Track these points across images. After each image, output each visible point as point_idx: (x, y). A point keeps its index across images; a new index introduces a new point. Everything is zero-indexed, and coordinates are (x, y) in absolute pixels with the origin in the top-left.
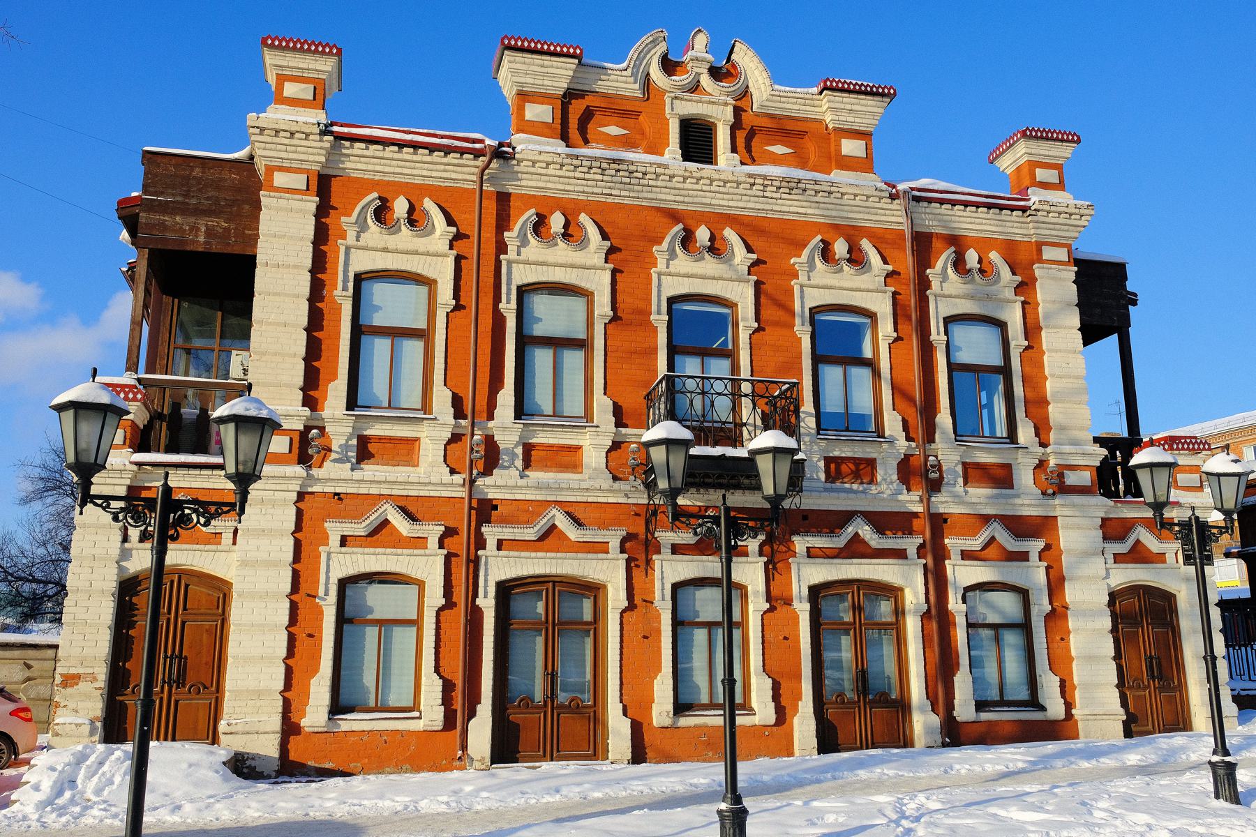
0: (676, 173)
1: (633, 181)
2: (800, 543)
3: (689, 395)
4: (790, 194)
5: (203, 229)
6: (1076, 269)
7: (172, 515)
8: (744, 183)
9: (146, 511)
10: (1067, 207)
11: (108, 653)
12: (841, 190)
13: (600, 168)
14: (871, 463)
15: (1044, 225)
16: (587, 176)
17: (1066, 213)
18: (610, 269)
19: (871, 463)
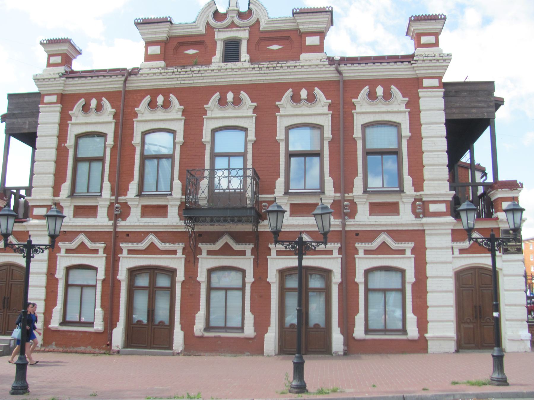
1: (194, 75)
3: (218, 178)
4: (273, 70)
5: (27, 123)
6: (443, 90)
7: (303, 247)
8: (249, 68)
9: (295, 245)
10: (435, 56)
11: (61, 309)
12: (301, 64)
13: (178, 72)
14: (165, 207)
15: (422, 68)
16: (172, 76)
17: (434, 60)
18: (255, 116)
19: (165, 207)
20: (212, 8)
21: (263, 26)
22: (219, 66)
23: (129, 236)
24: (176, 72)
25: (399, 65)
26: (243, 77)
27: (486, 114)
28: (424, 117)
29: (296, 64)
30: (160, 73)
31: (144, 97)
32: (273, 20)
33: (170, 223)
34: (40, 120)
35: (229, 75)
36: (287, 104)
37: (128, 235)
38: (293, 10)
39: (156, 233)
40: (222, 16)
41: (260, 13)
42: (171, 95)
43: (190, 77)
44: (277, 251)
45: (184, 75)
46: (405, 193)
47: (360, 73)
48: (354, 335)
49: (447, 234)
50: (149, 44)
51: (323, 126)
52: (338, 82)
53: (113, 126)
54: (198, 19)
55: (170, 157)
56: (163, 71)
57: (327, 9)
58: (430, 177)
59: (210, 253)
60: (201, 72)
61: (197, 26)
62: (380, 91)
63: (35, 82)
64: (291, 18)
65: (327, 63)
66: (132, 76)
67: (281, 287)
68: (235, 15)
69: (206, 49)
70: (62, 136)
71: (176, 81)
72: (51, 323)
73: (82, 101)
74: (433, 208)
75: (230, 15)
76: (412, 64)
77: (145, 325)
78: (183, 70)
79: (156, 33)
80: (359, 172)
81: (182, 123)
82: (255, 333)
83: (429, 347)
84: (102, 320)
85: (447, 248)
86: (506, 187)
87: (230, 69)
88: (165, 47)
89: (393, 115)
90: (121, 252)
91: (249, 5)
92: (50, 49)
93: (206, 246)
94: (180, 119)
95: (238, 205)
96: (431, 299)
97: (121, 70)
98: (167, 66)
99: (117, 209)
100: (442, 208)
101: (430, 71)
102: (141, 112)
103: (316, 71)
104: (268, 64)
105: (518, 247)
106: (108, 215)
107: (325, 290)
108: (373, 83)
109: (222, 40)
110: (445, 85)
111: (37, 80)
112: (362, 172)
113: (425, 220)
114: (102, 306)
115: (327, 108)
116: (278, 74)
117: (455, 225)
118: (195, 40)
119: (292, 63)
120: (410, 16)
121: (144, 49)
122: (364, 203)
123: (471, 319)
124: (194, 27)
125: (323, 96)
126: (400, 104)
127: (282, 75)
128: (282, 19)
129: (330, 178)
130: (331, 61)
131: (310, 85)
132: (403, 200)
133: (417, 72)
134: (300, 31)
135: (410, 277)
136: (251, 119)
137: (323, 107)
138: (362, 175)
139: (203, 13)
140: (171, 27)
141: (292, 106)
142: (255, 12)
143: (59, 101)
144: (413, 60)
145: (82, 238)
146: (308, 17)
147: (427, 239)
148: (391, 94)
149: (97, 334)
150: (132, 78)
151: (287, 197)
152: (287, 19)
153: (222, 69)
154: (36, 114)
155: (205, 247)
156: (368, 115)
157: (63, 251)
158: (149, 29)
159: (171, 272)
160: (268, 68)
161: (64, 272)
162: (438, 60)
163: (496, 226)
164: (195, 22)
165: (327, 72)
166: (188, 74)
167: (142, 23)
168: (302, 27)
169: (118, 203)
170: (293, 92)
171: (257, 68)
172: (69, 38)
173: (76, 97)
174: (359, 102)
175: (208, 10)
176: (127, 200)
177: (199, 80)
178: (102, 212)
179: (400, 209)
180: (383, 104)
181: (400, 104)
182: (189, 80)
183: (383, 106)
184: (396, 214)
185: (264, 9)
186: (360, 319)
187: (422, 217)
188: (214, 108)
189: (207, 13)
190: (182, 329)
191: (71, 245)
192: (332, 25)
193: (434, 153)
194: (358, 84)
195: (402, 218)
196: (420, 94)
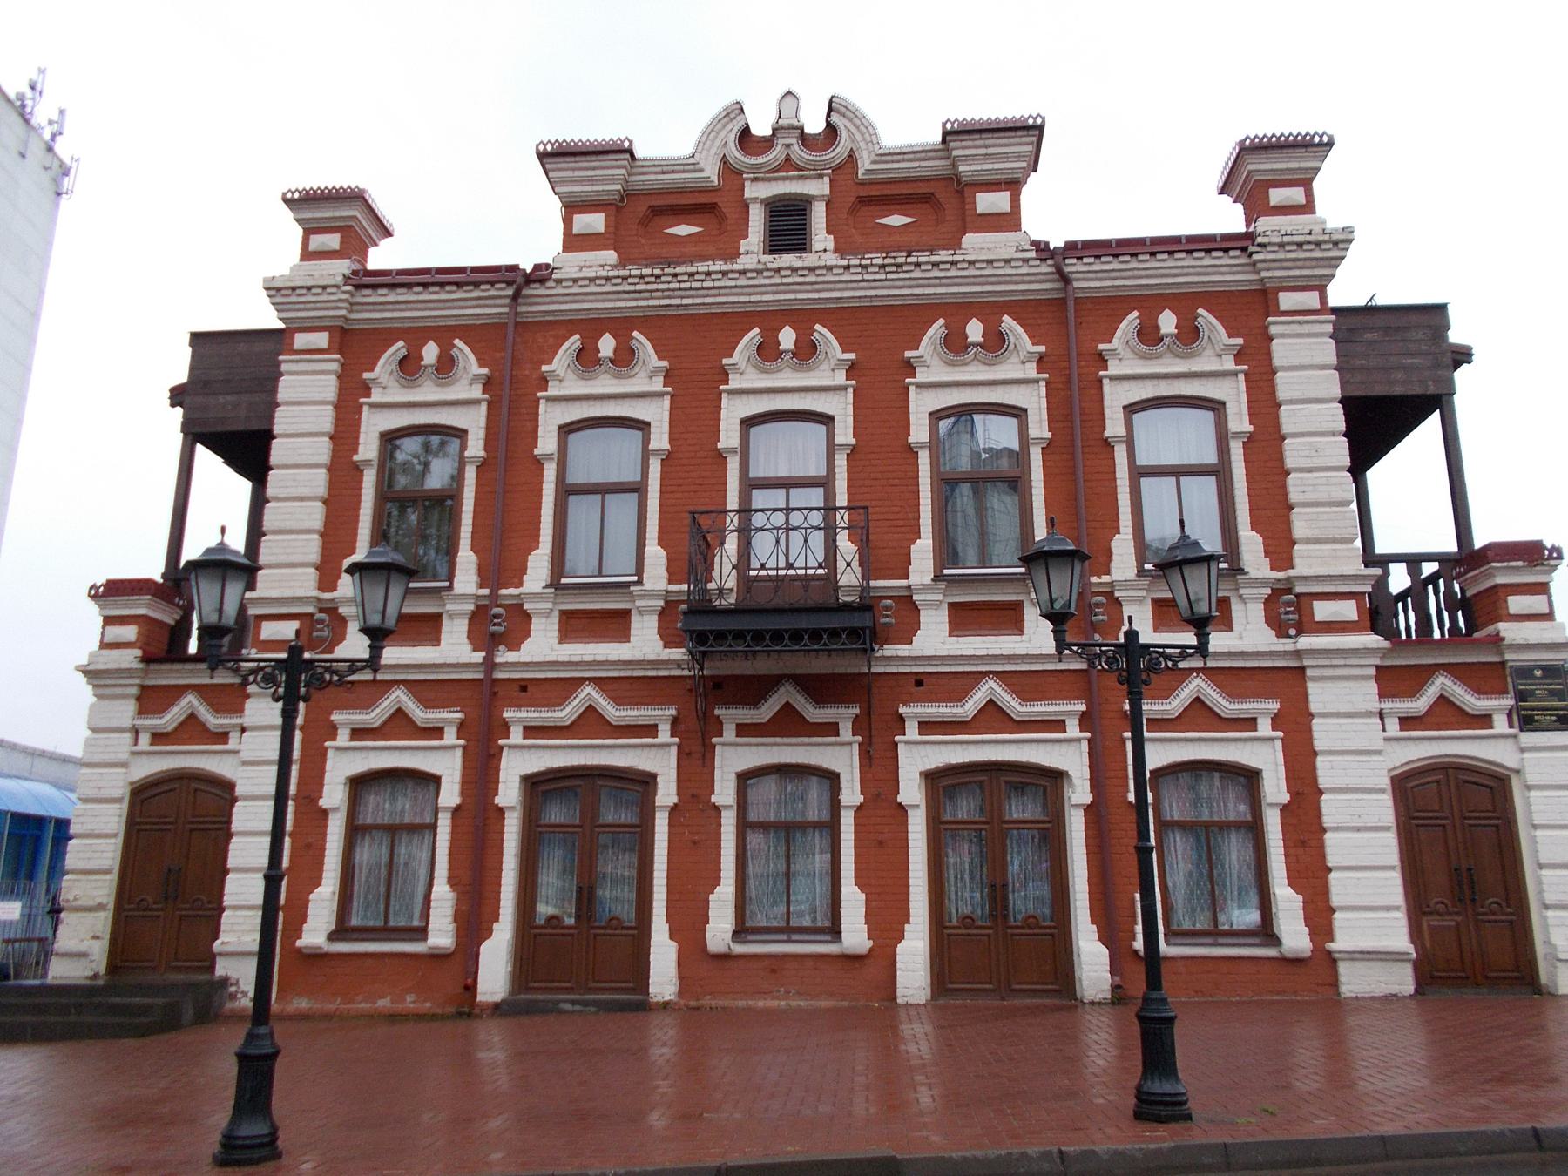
0: (746, 267)
1: (695, 285)
2: (913, 712)
3: (775, 531)
4: (897, 272)
10: (1310, 234)
12: (968, 258)
13: (652, 275)
14: (625, 614)
16: (638, 287)
17: (1309, 243)
20: (735, 122)
21: (865, 164)
22: (759, 262)
23: (528, 690)
24: (647, 276)
25: (1218, 259)
27: (1430, 383)
28: (1286, 385)
29: (956, 258)
30: (608, 279)
31: (566, 339)
32: (892, 151)
33: (638, 656)
34: (283, 393)
37: (919, 683)
38: (944, 125)
40: (760, 145)
41: (859, 137)
42: (635, 334)
43: (685, 289)
45: (669, 283)
46: (1246, 573)
49: (1364, 678)
50: (572, 207)
51: (1025, 410)
52: (1062, 302)
54: (699, 150)
56: (615, 273)
57: (1031, 122)
58: (1310, 533)
59: (743, 730)
60: (713, 276)
61: (697, 166)
62: (1168, 322)
63: (269, 296)
64: (937, 147)
65: (1033, 254)
66: (532, 286)
67: (934, 818)
68: (794, 141)
69: (720, 223)
70: (344, 434)
71: (648, 299)
72: (304, 935)
73: (398, 348)
74: (1323, 611)
75: (781, 141)
76: (1252, 253)
77: (569, 927)
78: (666, 271)
80: (1122, 523)
81: (666, 402)
82: (870, 943)
83: (1342, 979)
84: (450, 919)
85: (1369, 714)
86: (1516, 557)
87: (787, 268)
89: (1204, 381)
90: (505, 730)
91: (828, 115)
92: (309, 215)
94: (660, 395)
95: (814, 599)
96: (1336, 847)
97: (504, 269)
98: (622, 264)
99: (495, 621)
100: (1348, 611)
101: (1297, 273)
102: (558, 375)
103: (1005, 275)
104: (884, 258)
105: (1561, 712)
106: (469, 638)
108: (1150, 303)
109: (762, 201)
110: (1336, 311)
111: (275, 290)
112: (1130, 523)
113: (1306, 642)
114: (452, 881)
115: (1034, 365)
116: (907, 283)
117: (1384, 653)
119: (943, 256)
120: (1243, 137)
121: (561, 225)
122: (1140, 601)
123: (1449, 905)
124: (691, 167)
125: (1025, 337)
126: (1220, 356)
128: (915, 149)
130: (1042, 248)
131: (990, 310)
132: (1242, 591)
133: (1264, 274)
134: (959, 182)
135: (1275, 789)
136: (843, 393)
137: (1023, 363)
138: (1130, 530)
139: (713, 134)
141: (945, 362)
142: (844, 134)
143: (337, 346)
144: (1253, 245)
146: (981, 142)
147: (1313, 689)
148: (1196, 332)
149: (437, 957)
150: (536, 290)
151: (942, 585)
152: (927, 148)
153: (768, 270)
154: (272, 378)
155: (731, 716)
156: (1140, 383)
158: (573, 169)
160: (883, 266)
161: (345, 791)
163: (1496, 659)
164: (693, 156)
165: (1033, 278)
166: (680, 282)
167: (554, 157)
168: (966, 168)
170: (946, 325)
171: (856, 266)
172: (361, 187)
173: (381, 337)
174: (1115, 350)
175: (724, 126)
176: (522, 599)
177: (707, 296)
179: (1234, 614)
180: (1177, 356)
181: (1220, 356)
182: (682, 297)
183: (1178, 360)
184: (435, 643)
185: (867, 124)
187: (1296, 636)
189: (723, 133)
190: (672, 936)
191: (367, 717)
192: (1035, 171)
193: (1315, 475)
194: (1114, 306)
195: (1241, 638)
196: (1273, 330)
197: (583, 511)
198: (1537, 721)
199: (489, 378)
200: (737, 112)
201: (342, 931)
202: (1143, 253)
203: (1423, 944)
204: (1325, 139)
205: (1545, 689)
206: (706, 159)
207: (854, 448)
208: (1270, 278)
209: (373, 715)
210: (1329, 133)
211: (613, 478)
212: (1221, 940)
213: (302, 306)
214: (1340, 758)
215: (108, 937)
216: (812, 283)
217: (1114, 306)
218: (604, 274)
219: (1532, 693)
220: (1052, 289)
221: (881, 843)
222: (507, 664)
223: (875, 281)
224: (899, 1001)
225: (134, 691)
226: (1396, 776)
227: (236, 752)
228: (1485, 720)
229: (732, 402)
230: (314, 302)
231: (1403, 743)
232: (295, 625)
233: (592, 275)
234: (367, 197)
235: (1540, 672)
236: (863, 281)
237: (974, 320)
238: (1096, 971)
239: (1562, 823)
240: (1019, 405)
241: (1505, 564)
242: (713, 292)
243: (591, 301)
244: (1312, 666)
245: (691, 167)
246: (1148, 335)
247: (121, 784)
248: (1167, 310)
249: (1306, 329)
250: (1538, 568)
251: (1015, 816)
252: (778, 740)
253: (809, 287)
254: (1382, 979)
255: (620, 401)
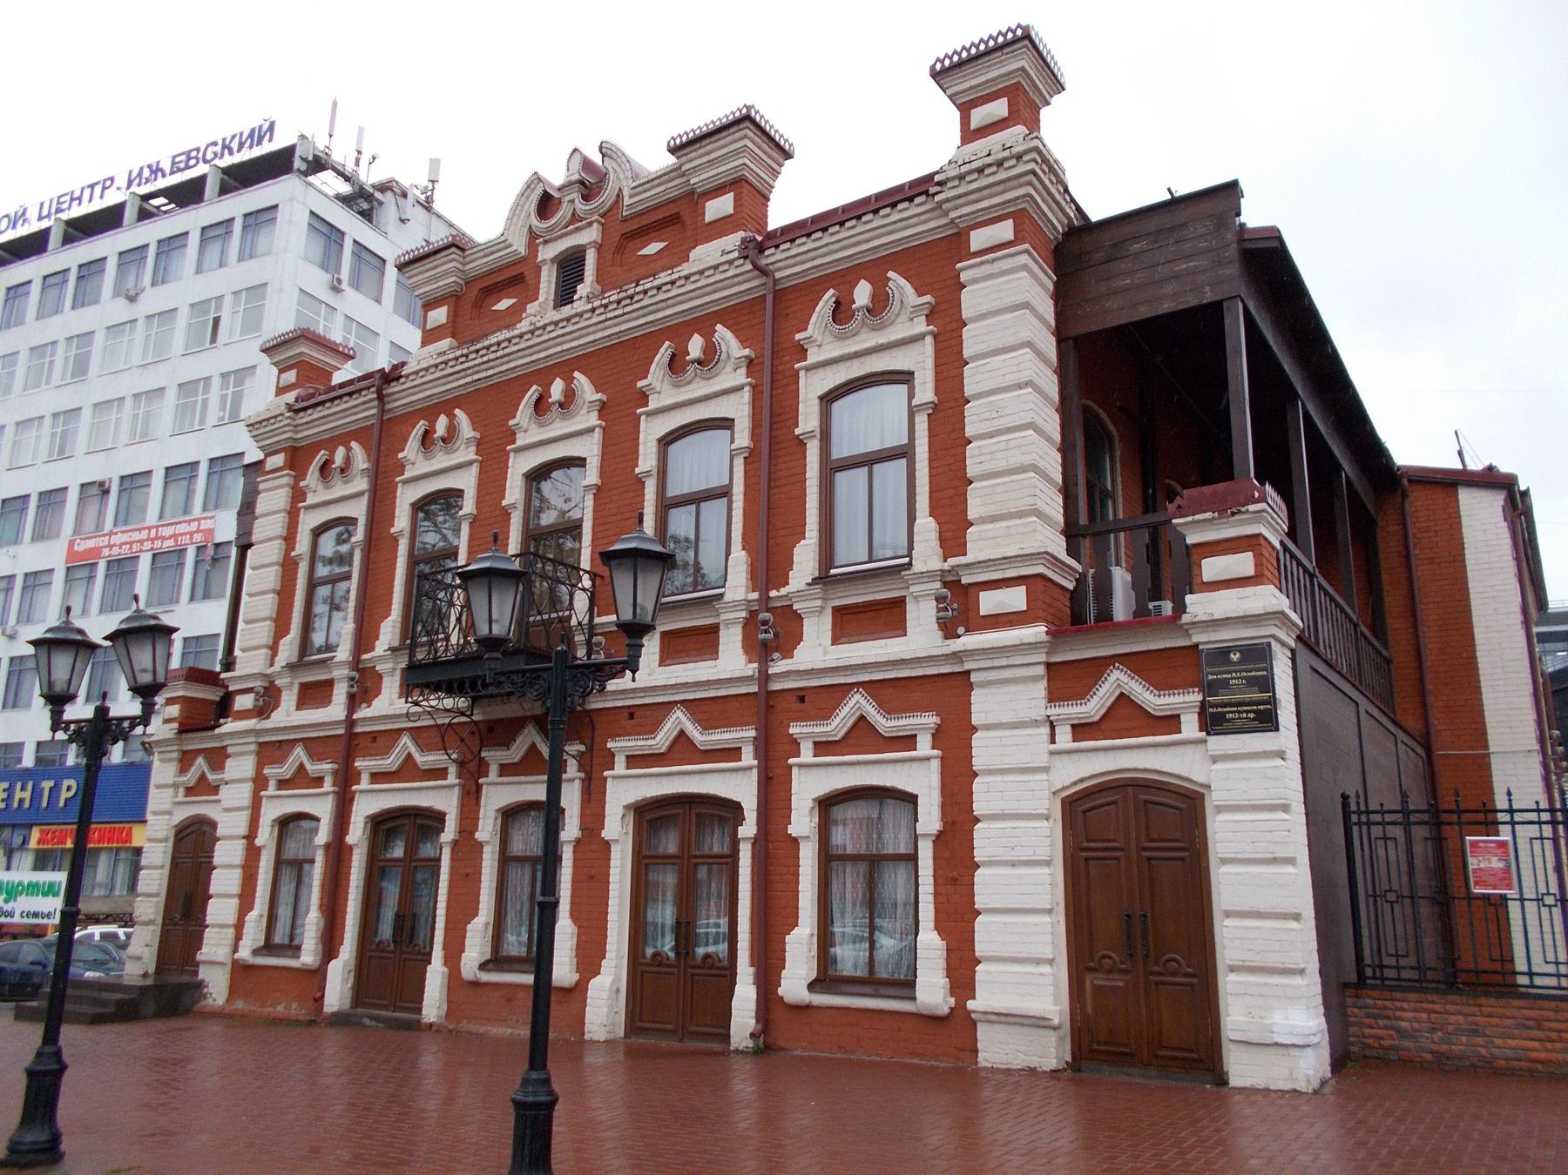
2: (621, 746)
10: (989, 155)
17: (990, 165)
23: (381, 740)
25: (906, 210)
26: (578, 338)
30: (436, 366)
35: (611, 319)
36: (663, 381)
37: (632, 716)
39: (870, 687)
44: (628, 757)
47: (814, 259)
48: (781, 991)
53: (746, 394)
55: (905, 452)
66: (392, 384)
68: (574, 196)
73: (533, 392)
74: (989, 602)
78: (472, 349)
79: (435, 279)
85: (1035, 723)
88: (456, 307)
93: (499, 753)
96: (987, 886)
105: (1262, 707)
107: (679, 861)
116: (641, 312)
118: (508, 276)
124: (503, 245)
127: (651, 313)
129: (744, 553)
133: (953, 215)
140: (464, 258)
145: (858, 704)
146: (702, 151)
147: (977, 697)
150: (395, 388)
153: (538, 329)
155: (495, 757)
156: (835, 368)
157: (272, 784)
159: (435, 819)
160: (619, 302)
162: (1000, 164)
169: (768, 610)
174: (811, 337)
175: (528, 198)
178: (731, 641)
184: (900, 632)
186: (800, 945)
188: (528, 426)
189: (527, 206)
194: (810, 290)
197: (850, 485)
198: (1229, 721)
199: (604, 403)
200: (536, 182)
201: (826, 979)
202: (865, 214)
203: (1083, 1008)
204: (1019, 32)
205: (1242, 678)
206: (514, 234)
207: (935, 407)
208: (960, 217)
209: (834, 725)
210: (1024, 24)
211: (874, 446)
212: (883, 991)
213: (654, 307)
214: (999, 778)
215: (157, 945)
216: (572, 332)
217: (810, 290)
218: (432, 362)
219: (1225, 684)
220: (758, 286)
221: (591, 877)
222: (364, 719)
223: (616, 317)
224: (587, 1037)
225: (253, 747)
226: (1067, 797)
227: (219, 801)
228: (1171, 723)
229: (650, 425)
230: (884, 226)
231: (1075, 756)
232: (1021, 591)
233: (425, 365)
234: (1033, 36)
235: (1238, 655)
236: (607, 320)
237: (862, 281)
238: (742, 1017)
239: (1253, 856)
240: (728, 416)
241: (1190, 519)
242: (505, 359)
243: (429, 389)
244: (232, 745)
245: (503, 245)
246: (676, 365)
247: (166, 827)
248: (862, 281)
249: (998, 266)
250: (1237, 517)
251: (716, 850)
252: (522, 778)
253: (593, 328)
254: (1021, 1048)
255: (447, 475)
